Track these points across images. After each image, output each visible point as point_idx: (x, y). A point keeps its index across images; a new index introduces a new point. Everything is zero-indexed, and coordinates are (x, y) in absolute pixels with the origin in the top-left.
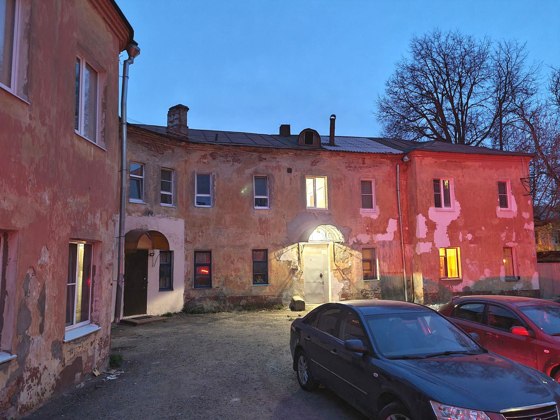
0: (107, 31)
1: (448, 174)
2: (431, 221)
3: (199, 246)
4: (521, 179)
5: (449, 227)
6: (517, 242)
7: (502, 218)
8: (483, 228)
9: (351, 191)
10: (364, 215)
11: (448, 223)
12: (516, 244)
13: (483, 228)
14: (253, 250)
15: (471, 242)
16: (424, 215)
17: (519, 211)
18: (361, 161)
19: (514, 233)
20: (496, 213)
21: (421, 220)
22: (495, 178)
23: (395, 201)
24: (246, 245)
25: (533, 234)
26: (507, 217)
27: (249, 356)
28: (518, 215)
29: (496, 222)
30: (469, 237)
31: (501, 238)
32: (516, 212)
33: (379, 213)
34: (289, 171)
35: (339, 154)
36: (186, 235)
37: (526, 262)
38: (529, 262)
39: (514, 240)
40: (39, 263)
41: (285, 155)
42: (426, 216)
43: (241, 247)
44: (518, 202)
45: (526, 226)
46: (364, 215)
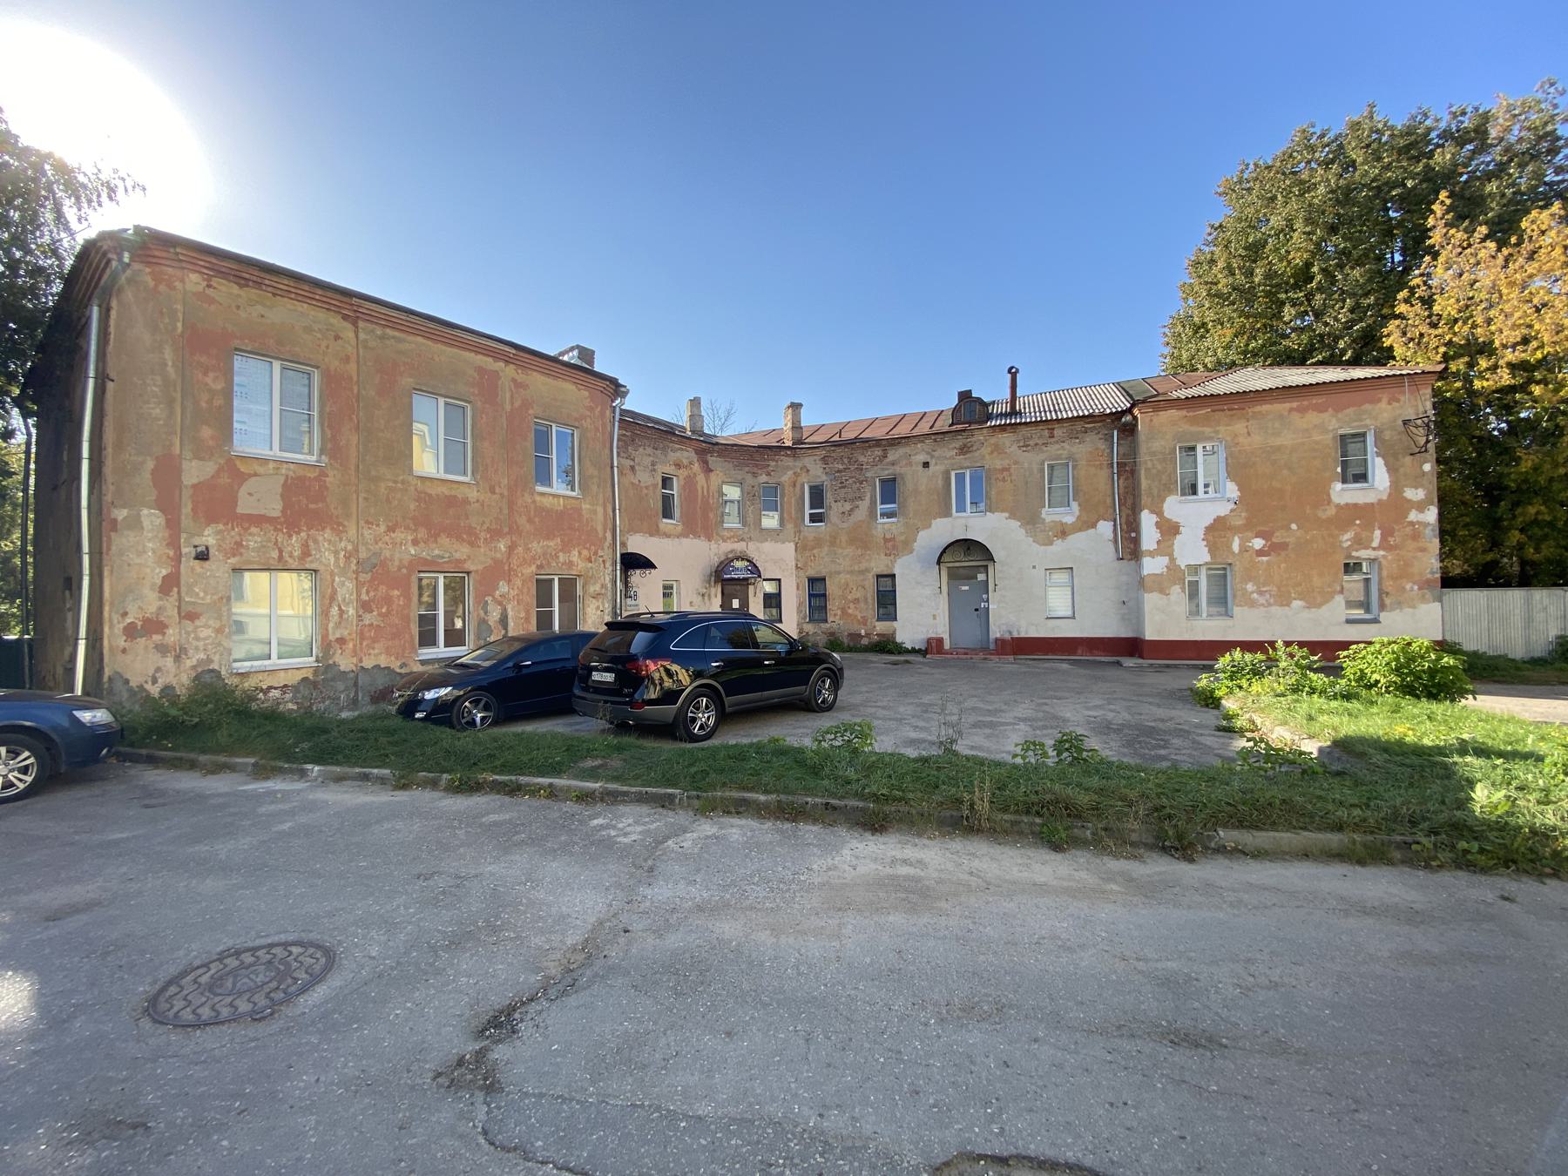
0: (579, 390)
1: (1213, 435)
2: (1168, 521)
3: (812, 573)
4: (1405, 422)
5: (1210, 530)
6: (1384, 549)
7: (1347, 504)
8: (1294, 526)
9: (1027, 483)
10: (1048, 519)
11: (1209, 521)
12: (1382, 553)
13: (1294, 526)
14: (879, 576)
15: (1260, 553)
16: (1152, 512)
17: (1396, 487)
18: (1046, 433)
19: (1377, 533)
20: (1329, 495)
21: (1147, 520)
22: (1331, 428)
23: (1109, 492)
24: (867, 570)
25: (1433, 530)
26: (1361, 502)
27: (585, 745)
28: (1390, 495)
29: (1331, 511)
30: (1258, 543)
31: (1341, 542)
32: (1385, 489)
33: (1077, 513)
34: (926, 465)
35: (1005, 430)
36: (797, 560)
37: (1408, 587)
38: (1416, 587)
39: (1375, 544)
40: (1513, 381)
41: (919, 446)
42: (1159, 512)
43: (862, 572)
44: (1391, 469)
45: (1413, 516)
46: (1048, 519)
